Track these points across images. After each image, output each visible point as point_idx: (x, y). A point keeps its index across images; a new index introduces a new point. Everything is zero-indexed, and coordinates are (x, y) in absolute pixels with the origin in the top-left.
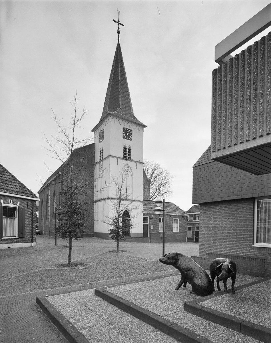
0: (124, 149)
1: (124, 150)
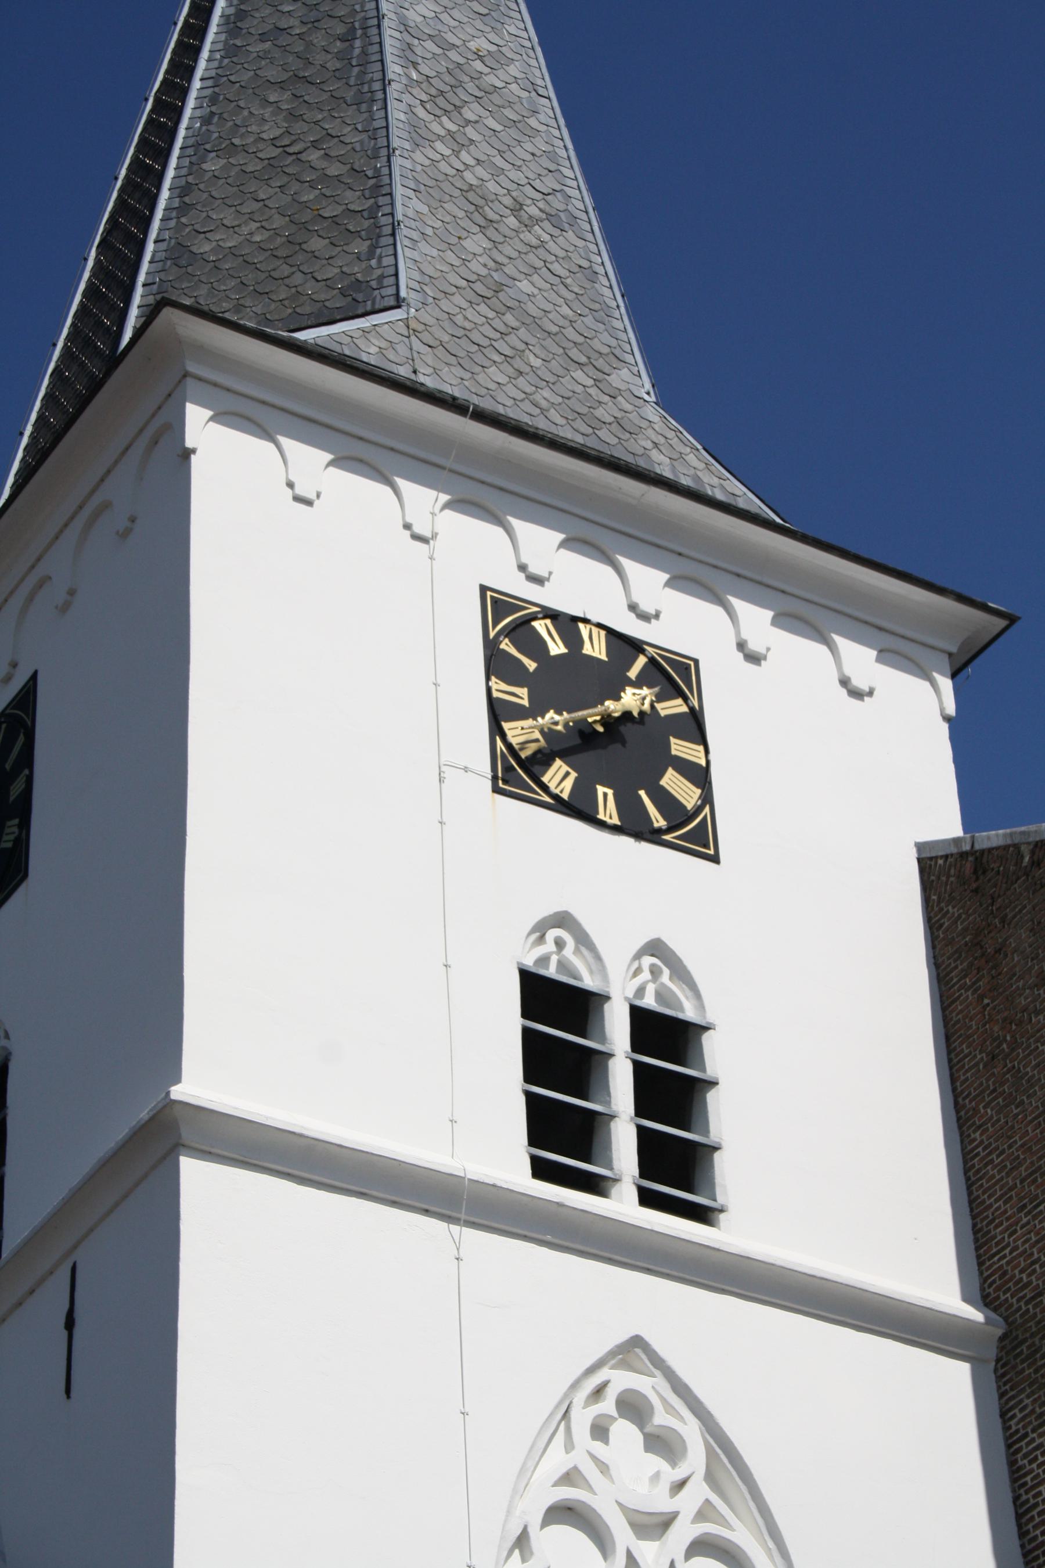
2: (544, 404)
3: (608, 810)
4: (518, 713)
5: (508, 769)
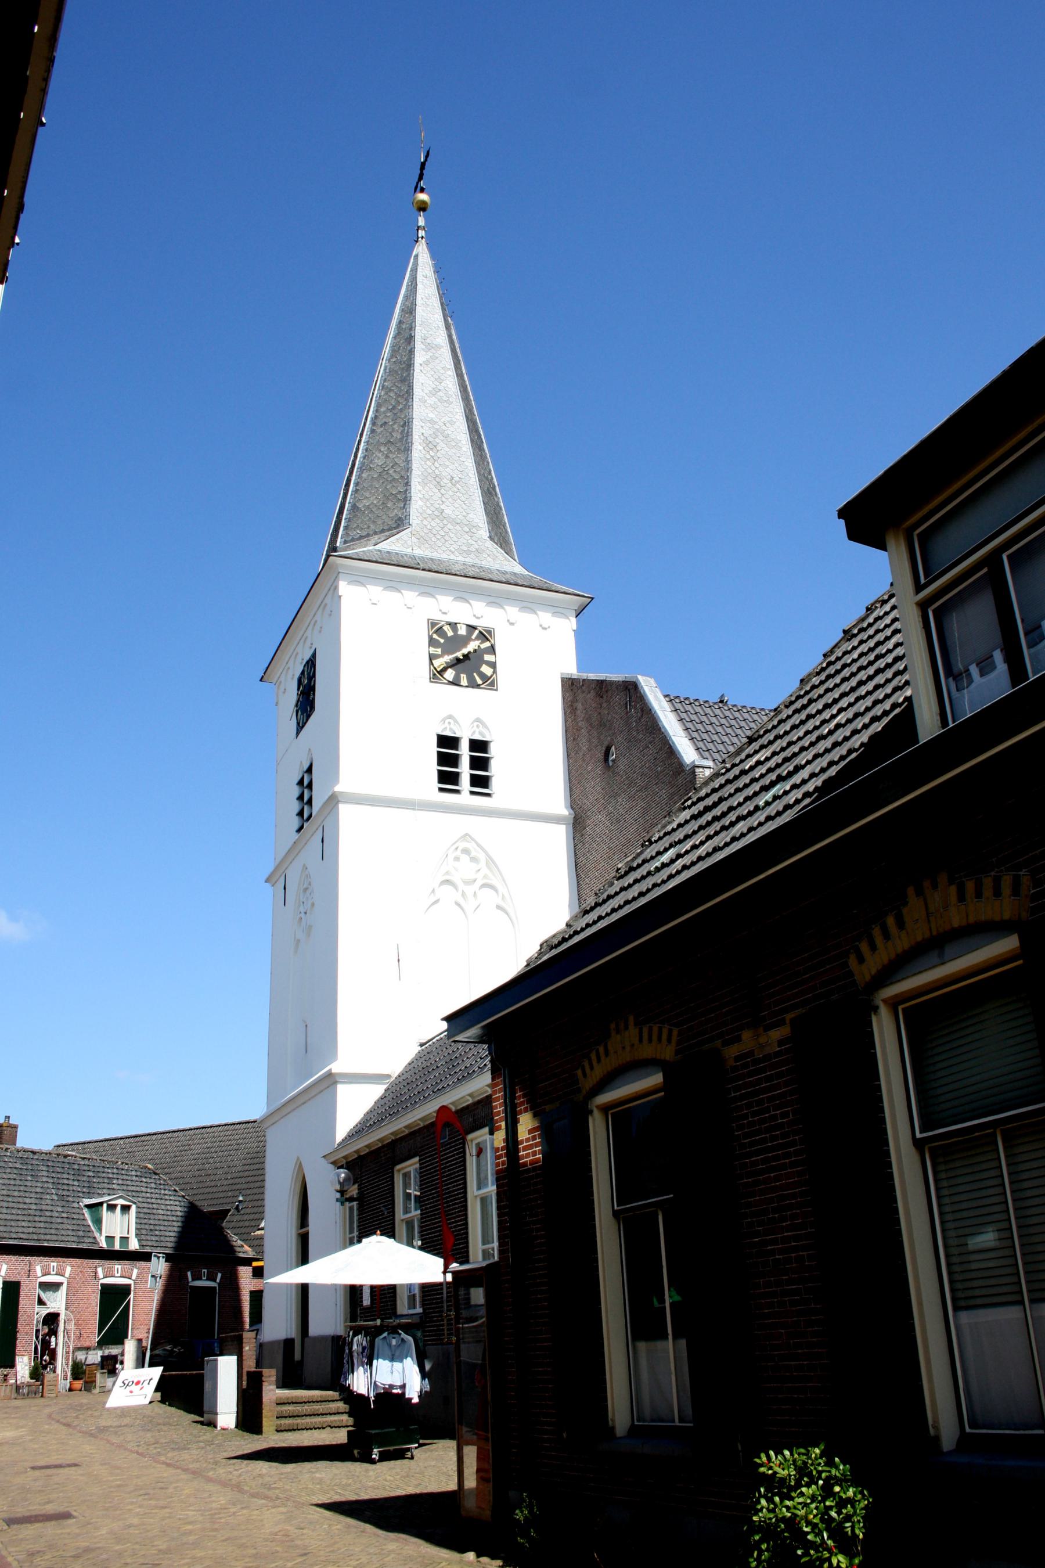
0: (439, 745)
2: (453, 550)
3: (464, 681)
4: (437, 657)
5: (434, 675)
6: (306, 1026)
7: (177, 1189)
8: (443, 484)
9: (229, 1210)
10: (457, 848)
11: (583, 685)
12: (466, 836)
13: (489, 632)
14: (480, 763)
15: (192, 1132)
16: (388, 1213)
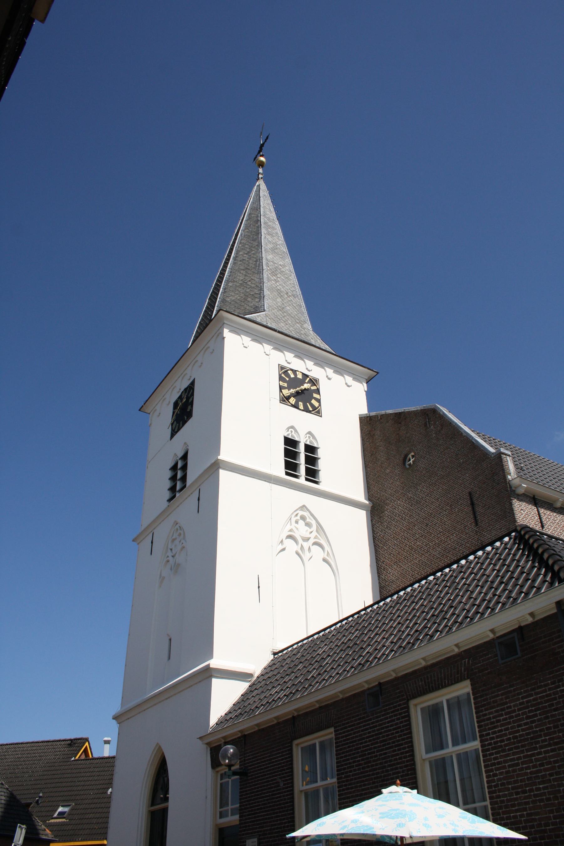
1: (286, 462)
2: (291, 330)
3: (301, 407)
6: (170, 640)
7: (4, 783)
8: (282, 295)
9: (31, 803)
10: (297, 515)
11: (381, 419)
12: (303, 507)
13: (316, 381)
14: (312, 460)
15: (7, 747)
16: (284, 785)
